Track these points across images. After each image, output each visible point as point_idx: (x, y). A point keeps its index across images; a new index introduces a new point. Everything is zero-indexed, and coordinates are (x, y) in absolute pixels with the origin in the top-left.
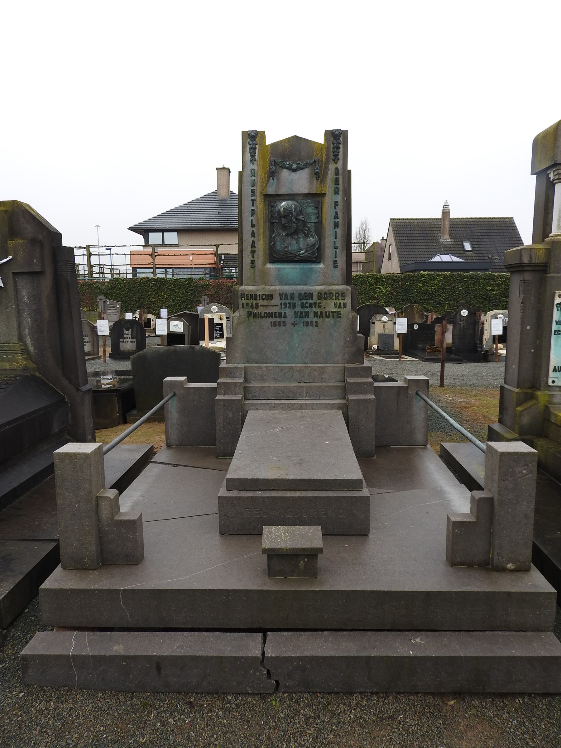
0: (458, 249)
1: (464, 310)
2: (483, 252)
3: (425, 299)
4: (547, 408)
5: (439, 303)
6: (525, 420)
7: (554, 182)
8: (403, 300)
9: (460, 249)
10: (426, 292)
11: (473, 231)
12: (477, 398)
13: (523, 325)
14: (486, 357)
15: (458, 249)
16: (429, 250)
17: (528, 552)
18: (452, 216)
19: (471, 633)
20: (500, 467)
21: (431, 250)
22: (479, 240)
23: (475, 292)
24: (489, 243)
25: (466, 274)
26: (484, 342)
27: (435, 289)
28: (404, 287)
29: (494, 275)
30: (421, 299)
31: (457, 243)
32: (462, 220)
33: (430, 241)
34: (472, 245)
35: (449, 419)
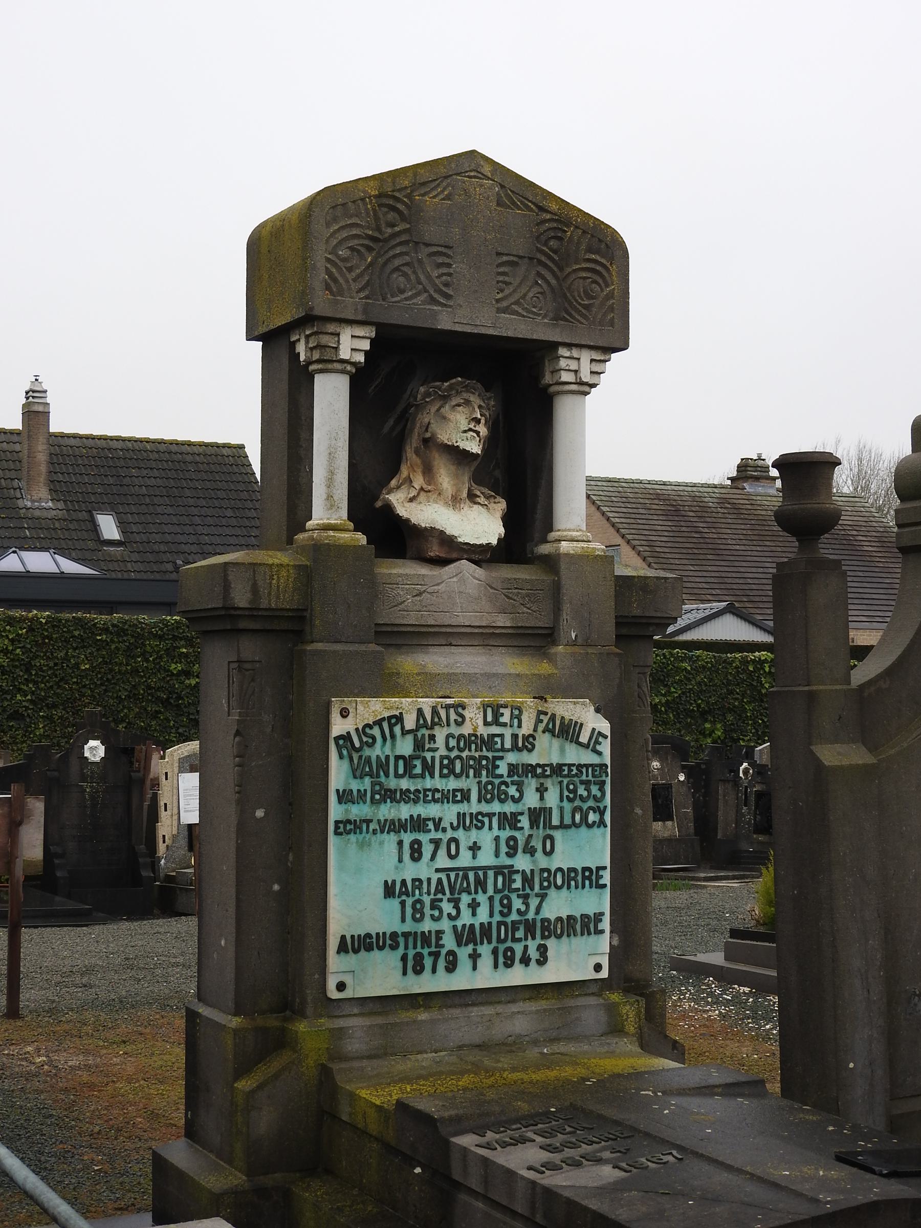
1: (93, 743)
2: (156, 547)
4: (325, 1073)
5: (16, 716)
6: (265, 1121)
7: (311, 368)
9: (85, 535)
11: (127, 481)
12: (129, 1048)
13: (244, 804)
14: (164, 899)
18: (54, 428)
22: (144, 509)
24: (175, 520)
25: (102, 619)
26: (161, 848)
32: (90, 443)
34: (122, 525)
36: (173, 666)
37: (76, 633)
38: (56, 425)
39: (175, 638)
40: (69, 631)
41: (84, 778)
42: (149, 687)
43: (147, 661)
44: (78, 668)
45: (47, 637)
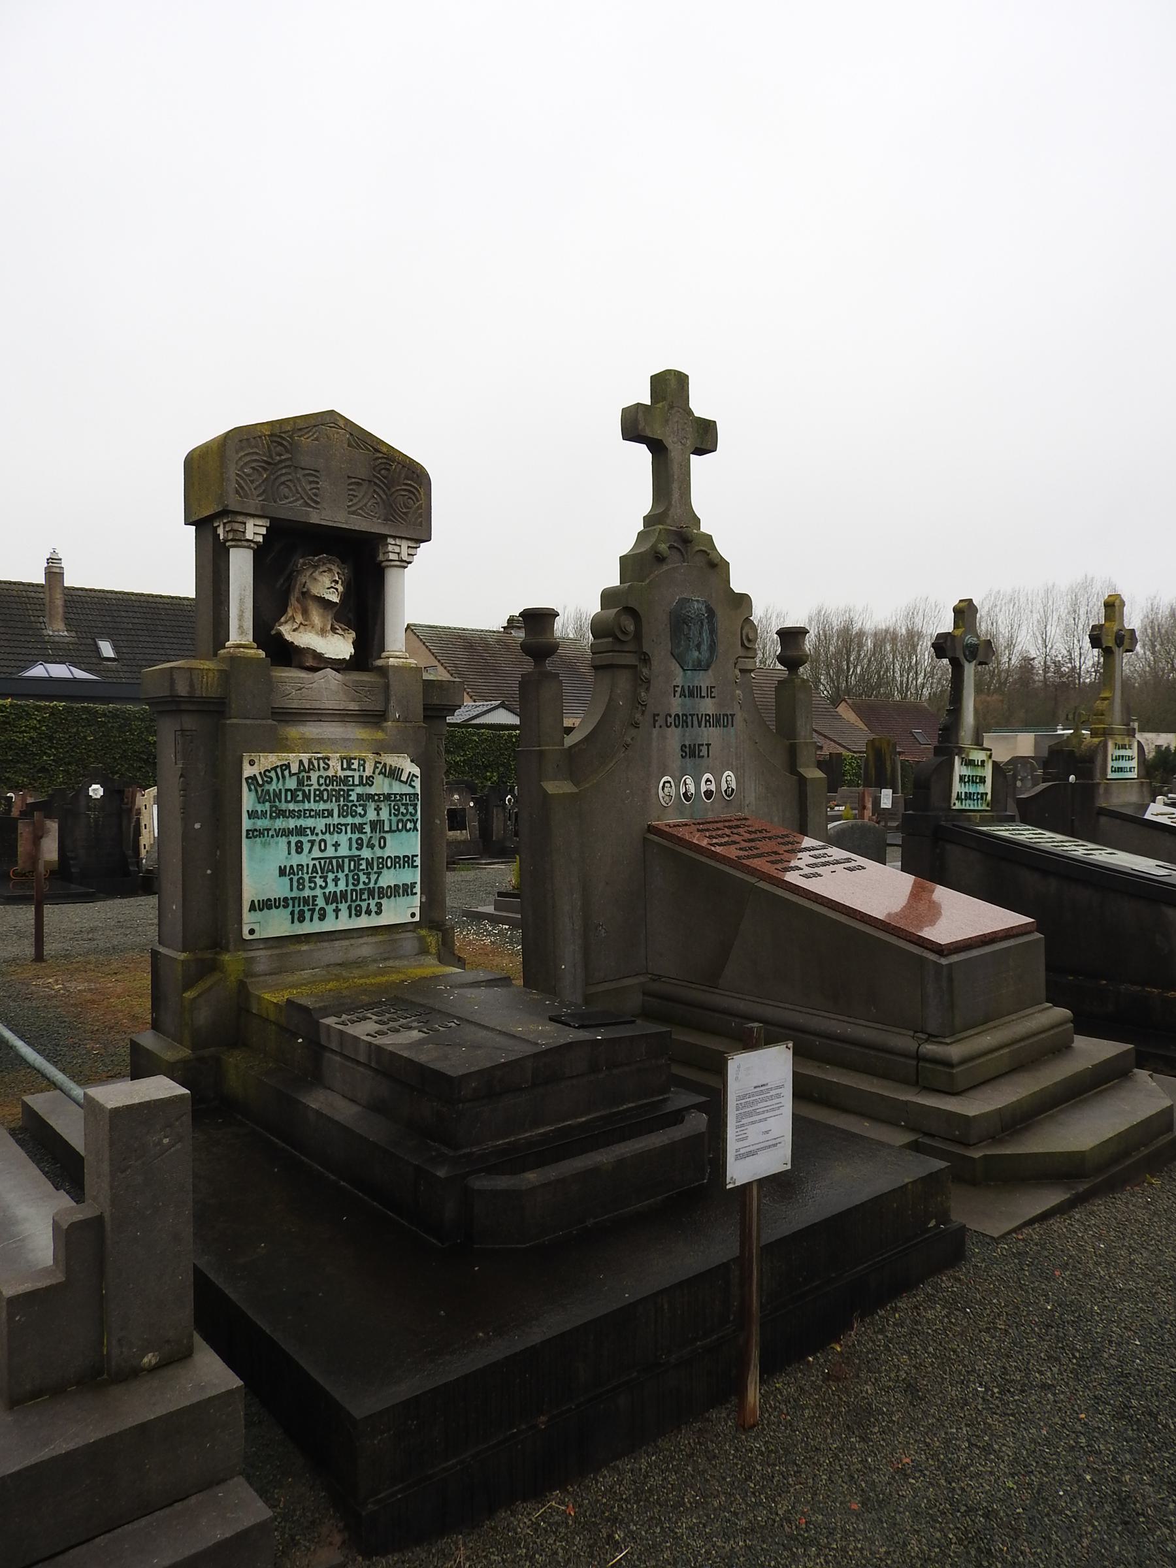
4: (242, 985)
5: (43, 770)
6: (203, 1017)
9: (91, 654)
11: (118, 620)
12: (119, 977)
13: (186, 821)
14: (146, 884)
17: (186, 1314)
18: (67, 583)
19: (60, 1558)
20: (112, 1144)
21: (24, 651)
22: (130, 638)
23: (125, 747)
25: (100, 707)
26: (143, 853)
27: (31, 738)
31: (84, 641)
34: (115, 648)
35: (20, 1045)
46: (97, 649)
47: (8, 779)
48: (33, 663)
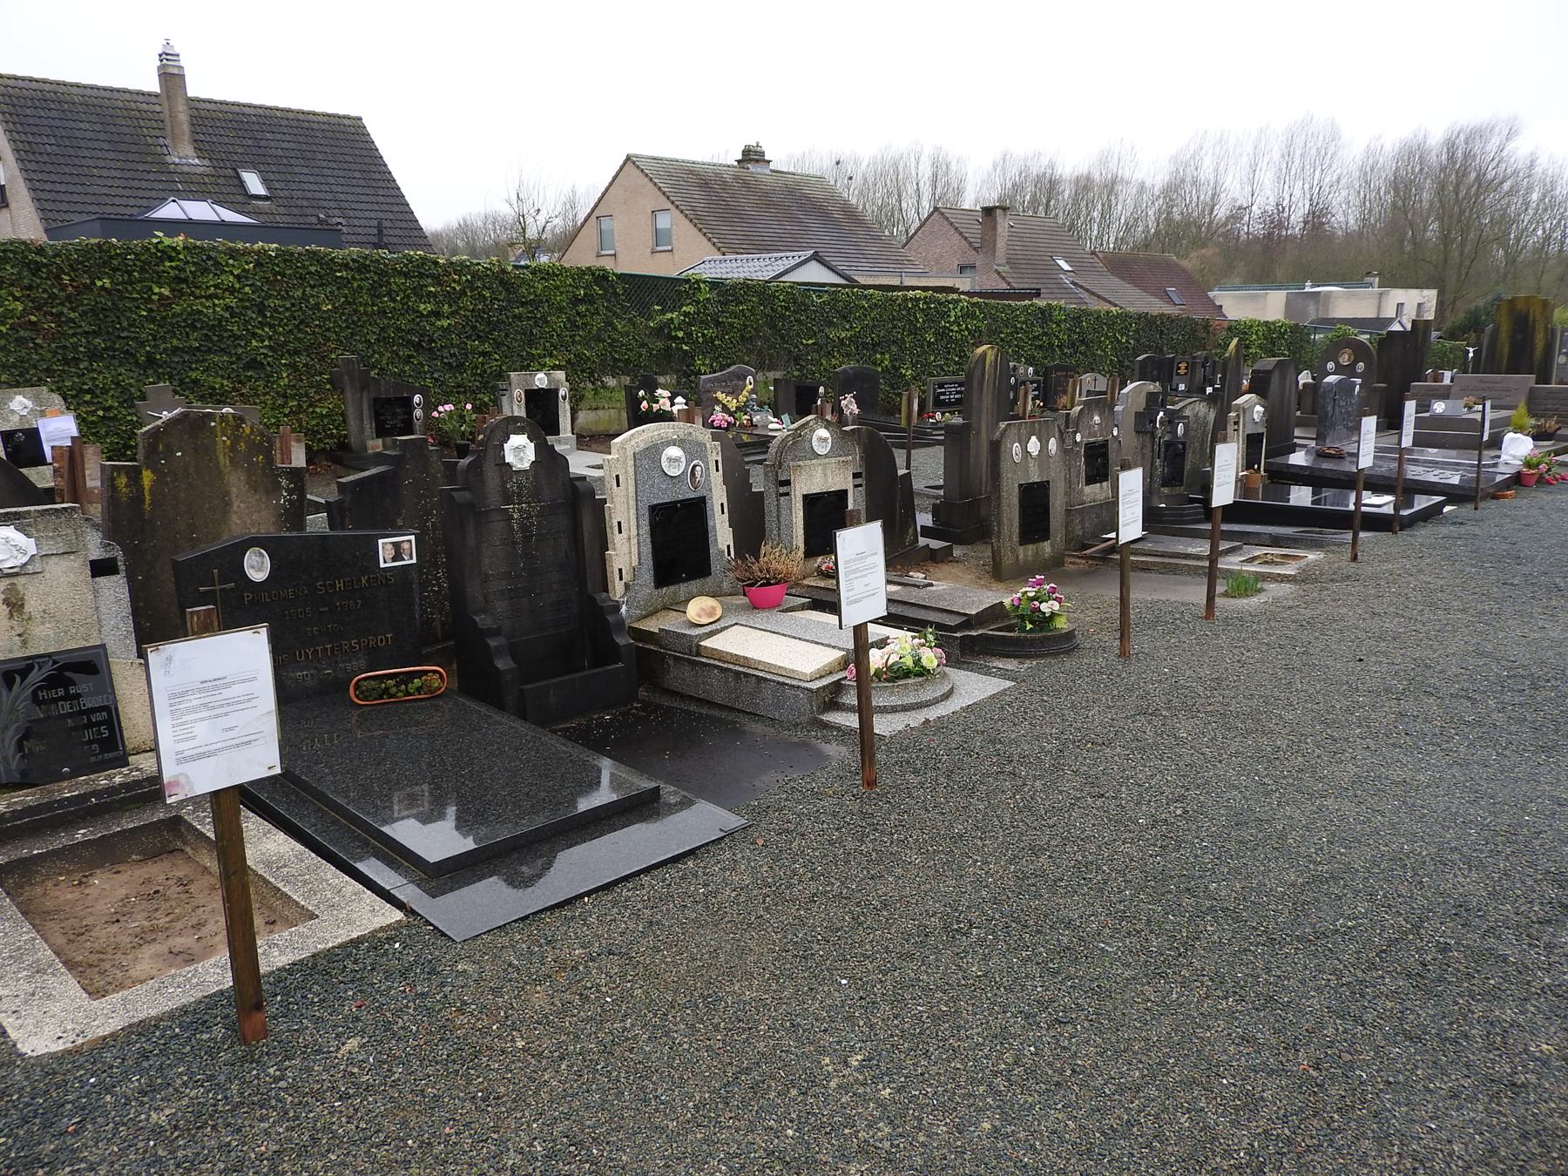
0: (229, 189)
2: (299, 202)
3: (193, 351)
5: (254, 364)
8: (93, 355)
10: (193, 322)
11: (263, 143)
15: (229, 189)
16: (136, 184)
18: (190, 94)
21: (144, 184)
22: (282, 168)
27: (227, 308)
28: (86, 299)
29: (436, 263)
30: (175, 350)
31: (221, 172)
33: (137, 157)
34: (265, 181)
36: (422, 307)
37: (313, 269)
38: (195, 88)
39: (421, 275)
40: (303, 267)
41: (508, 499)
42: (399, 329)
43: (394, 300)
44: (319, 309)
45: (279, 273)
46: (242, 184)
47: (196, 381)
48: (162, 201)
